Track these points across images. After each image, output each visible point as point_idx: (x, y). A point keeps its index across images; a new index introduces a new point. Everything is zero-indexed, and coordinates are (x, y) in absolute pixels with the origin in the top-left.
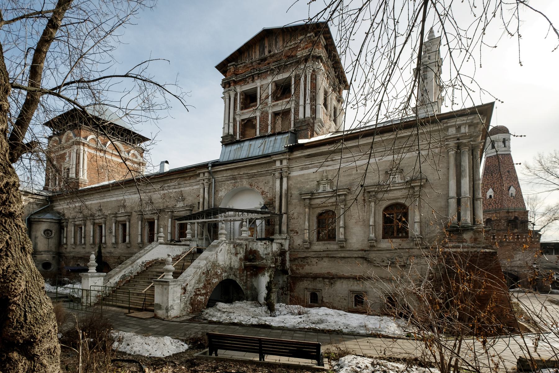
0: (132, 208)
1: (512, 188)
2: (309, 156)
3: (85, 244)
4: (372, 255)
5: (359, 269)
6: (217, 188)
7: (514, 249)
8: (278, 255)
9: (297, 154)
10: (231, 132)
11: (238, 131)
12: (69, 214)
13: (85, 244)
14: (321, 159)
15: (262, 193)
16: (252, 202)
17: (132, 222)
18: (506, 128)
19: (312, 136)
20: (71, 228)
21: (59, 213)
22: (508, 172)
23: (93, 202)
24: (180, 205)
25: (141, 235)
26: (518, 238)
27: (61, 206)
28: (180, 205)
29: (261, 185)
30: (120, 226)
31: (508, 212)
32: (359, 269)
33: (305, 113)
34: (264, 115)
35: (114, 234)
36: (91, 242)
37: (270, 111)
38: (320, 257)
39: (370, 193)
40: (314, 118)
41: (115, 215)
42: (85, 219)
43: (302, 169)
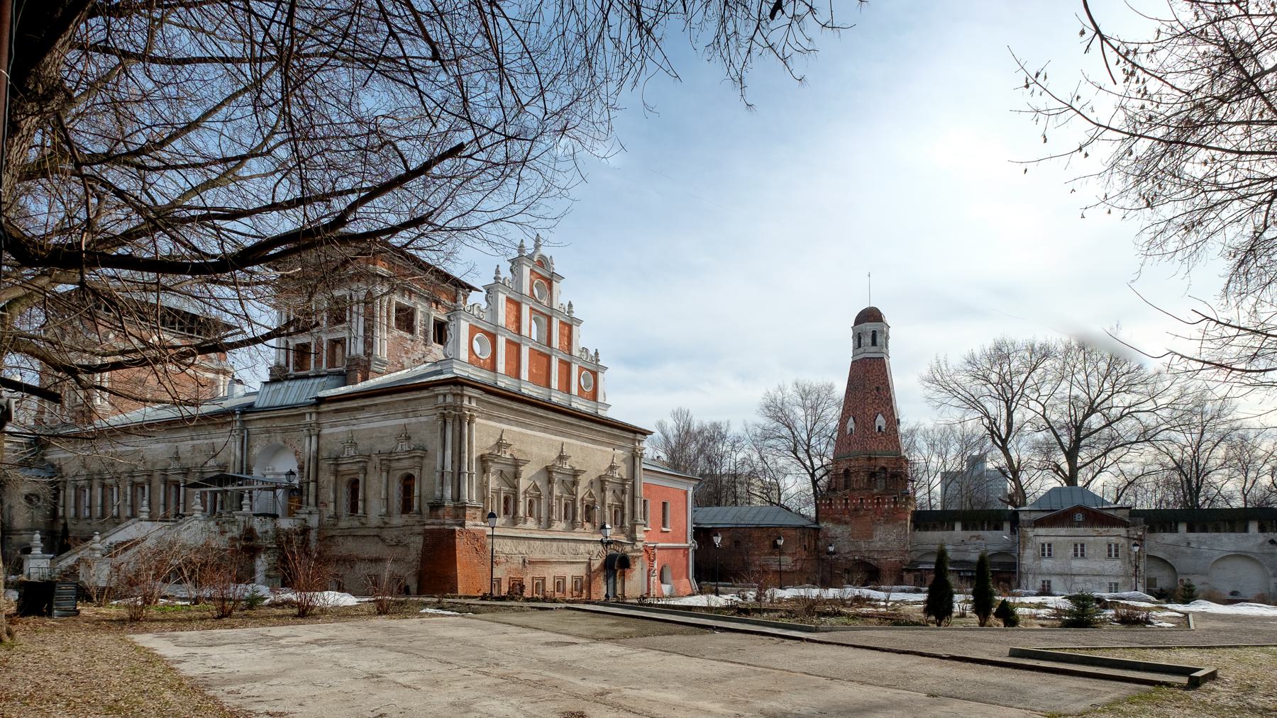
0: (154, 464)
1: (880, 418)
2: (337, 411)
3: (90, 517)
4: (385, 533)
5: (372, 549)
6: (252, 443)
7: (874, 523)
8: (296, 534)
9: (324, 408)
10: (283, 362)
11: (291, 360)
12: (71, 469)
13: (90, 517)
14: (346, 416)
15: (296, 453)
16: (285, 464)
17: (153, 485)
18: (880, 314)
19: (365, 378)
20: (71, 492)
21: (53, 466)
22: (878, 389)
23: (105, 450)
24: (212, 462)
25: (165, 505)
26: (878, 503)
27: (58, 454)
28: (212, 462)
29: (294, 443)
30: (173, 489)
31: (870, 459)
32: (372, 549)
33: (358, 349)
34: (319, 339)
35: (129, 503)
36: (99, 514)
37: (325, 339)
38: (350, 534)
39: (387, 460)
40: (370, 355)
41: (131, 474)
42: (90, 480)
43: (332, 427)
